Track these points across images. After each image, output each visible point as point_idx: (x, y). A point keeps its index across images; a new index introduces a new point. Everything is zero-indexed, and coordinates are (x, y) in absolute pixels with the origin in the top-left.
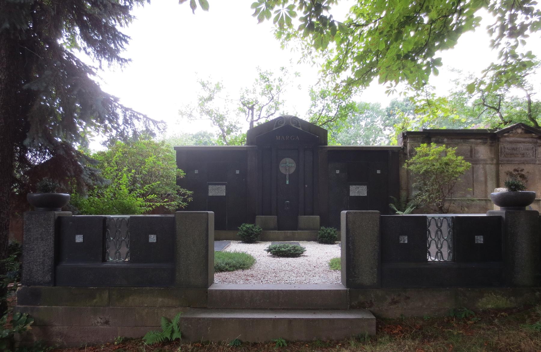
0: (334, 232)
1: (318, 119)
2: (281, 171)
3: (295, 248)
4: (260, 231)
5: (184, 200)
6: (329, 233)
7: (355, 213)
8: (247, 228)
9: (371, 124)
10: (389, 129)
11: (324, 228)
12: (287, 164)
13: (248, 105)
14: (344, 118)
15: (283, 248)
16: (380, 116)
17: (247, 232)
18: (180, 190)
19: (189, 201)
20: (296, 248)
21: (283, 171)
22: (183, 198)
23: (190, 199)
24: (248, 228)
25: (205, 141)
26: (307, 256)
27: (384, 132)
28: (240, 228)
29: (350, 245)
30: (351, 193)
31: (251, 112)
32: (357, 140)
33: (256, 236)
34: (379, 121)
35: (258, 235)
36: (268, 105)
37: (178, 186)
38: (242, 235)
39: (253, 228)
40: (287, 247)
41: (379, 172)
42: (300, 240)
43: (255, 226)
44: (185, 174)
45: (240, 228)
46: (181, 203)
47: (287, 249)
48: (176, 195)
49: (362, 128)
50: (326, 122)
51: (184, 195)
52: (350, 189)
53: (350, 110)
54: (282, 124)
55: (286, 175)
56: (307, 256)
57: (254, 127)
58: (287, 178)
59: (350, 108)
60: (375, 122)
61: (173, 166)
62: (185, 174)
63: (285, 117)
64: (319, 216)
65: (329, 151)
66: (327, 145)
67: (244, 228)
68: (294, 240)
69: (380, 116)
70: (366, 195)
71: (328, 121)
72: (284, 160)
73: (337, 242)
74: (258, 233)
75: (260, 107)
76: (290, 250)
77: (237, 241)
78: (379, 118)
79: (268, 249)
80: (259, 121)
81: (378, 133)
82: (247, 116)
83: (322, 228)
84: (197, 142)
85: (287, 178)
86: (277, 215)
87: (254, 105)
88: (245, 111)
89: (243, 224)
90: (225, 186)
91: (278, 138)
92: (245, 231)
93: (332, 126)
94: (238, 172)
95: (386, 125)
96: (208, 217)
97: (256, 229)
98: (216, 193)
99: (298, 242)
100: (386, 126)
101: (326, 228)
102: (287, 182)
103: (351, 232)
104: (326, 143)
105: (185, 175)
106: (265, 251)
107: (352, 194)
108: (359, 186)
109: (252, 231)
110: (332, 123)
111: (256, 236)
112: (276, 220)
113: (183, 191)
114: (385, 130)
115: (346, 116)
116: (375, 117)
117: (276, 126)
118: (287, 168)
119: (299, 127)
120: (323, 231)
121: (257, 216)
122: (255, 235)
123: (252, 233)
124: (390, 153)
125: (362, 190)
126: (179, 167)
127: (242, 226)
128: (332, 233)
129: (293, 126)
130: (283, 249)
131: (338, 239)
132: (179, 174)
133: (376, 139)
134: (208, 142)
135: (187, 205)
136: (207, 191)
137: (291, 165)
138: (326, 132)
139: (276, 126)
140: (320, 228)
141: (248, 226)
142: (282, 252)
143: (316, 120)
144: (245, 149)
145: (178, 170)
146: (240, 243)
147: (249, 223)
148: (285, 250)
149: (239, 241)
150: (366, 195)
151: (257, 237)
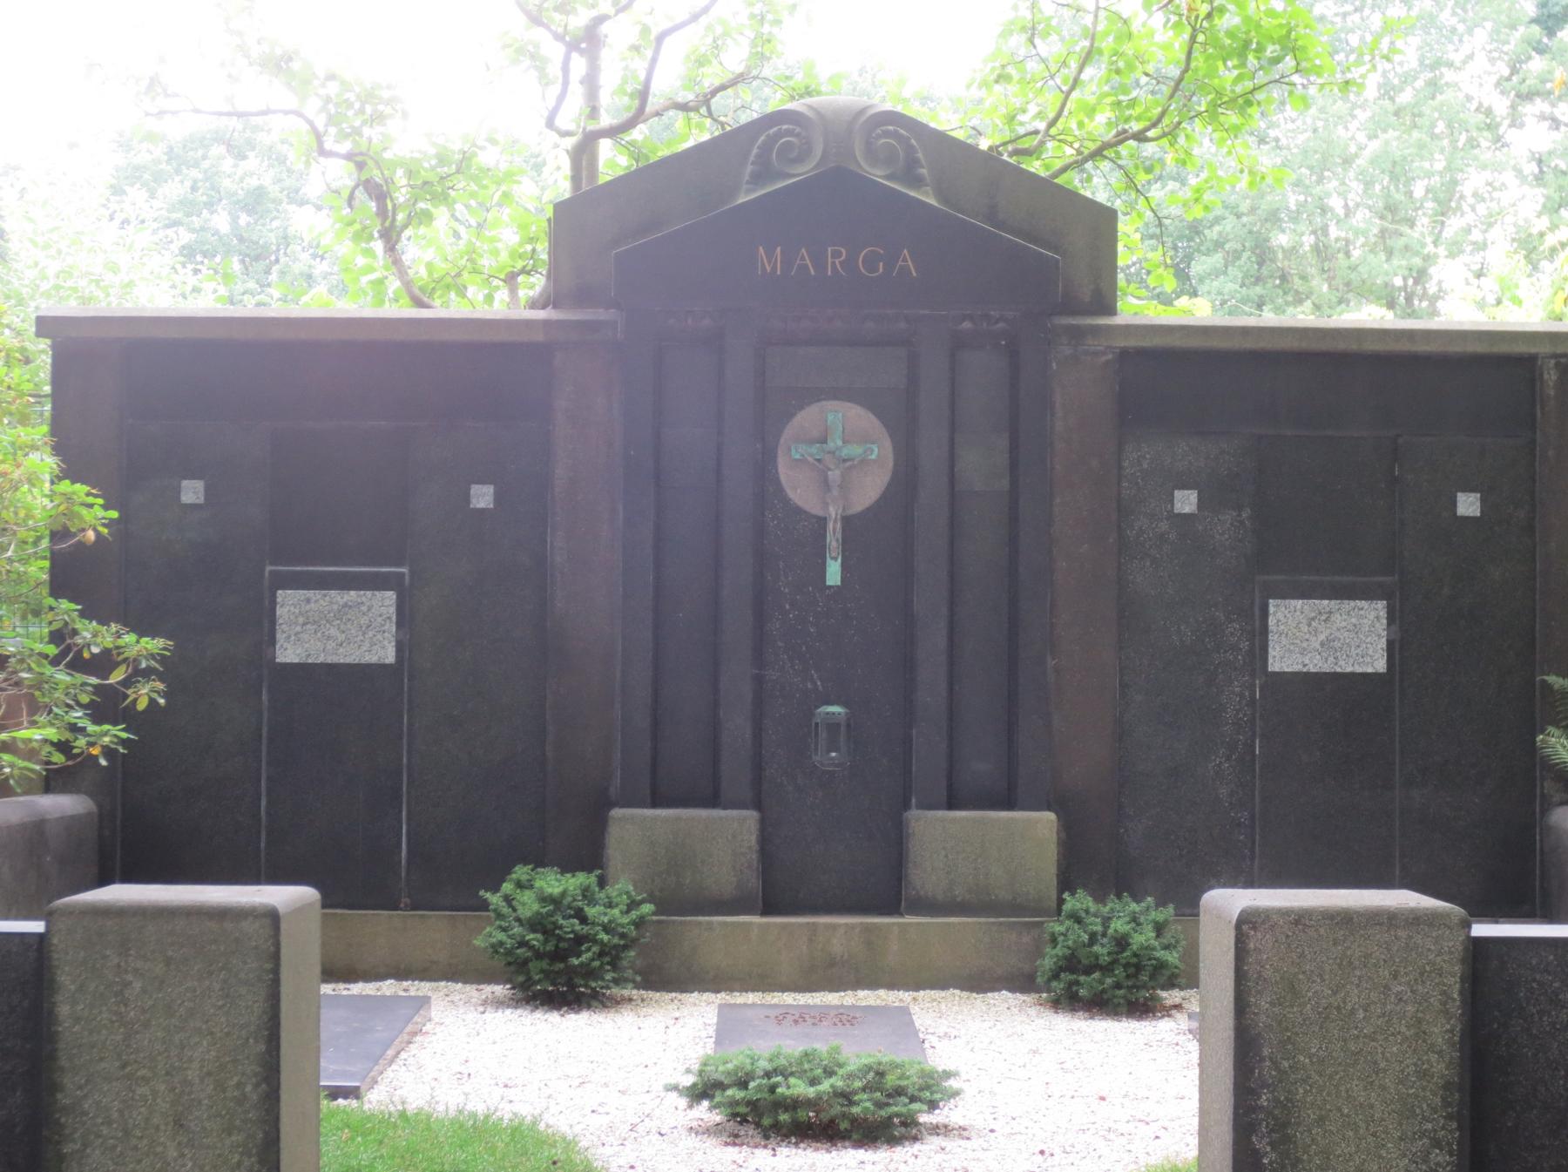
0: (1159, 929)
1: (1052, 123)
2: (791, 494)
3: (881, 1074)
4: (639, 923)
5: (107, 707)
6: (1122, 942)
7: (1297, 922)
8: (544, 899)
9: (1419, 83)
10: (1543, 117)
11: (1089, 903)
12: (831, 445)
13: (557, 16)
14: (1232, 118)
15: (801, 1074)
16: (1489, 25)
17: (545, 932)
18: (75, 632)
19: (142, 705)
20: (891, 1080)
21: (799, 489)
22: (94, 680)
23: (144, 695)
24: (555, 902)
25: (253, 182)
26: (962, 1132)
27: (1511, 135)
28: (495, 899)
29: (1260, 1143)
30: (1274, 652)
31: (579, 65)
32: (1329, 195)
33: (612, 956)
34: (1481, 60)
35: (626, 947)
36: (704, 20)
37: (65, 605)
38: (509, 952)
39: (592, 902)
40: (829, 1073)
41: (1468, 505)
42: (917, 985)
43: (602, 883)
44: (114, 514)
45: (495, 899)
46: (82, 730)
47: (825, 1086)
48: (49, 670)
49: (1363, 107)
50: (1107, 146)
51: (104, 663)
52: (1272, 621)
53: (1276, 61)
54: (800, 160)
55: (822, 522)
56: (962, 1132)
57: (603, 179)
58: (833, 538)
59: (1271, 50)
60: (1450, 65)
61: (34, 457)
62: (114, 514)
63: (818, 113)
64: (1051, 816)
65: (1124, 354)
66: (1111, 310)
67: (528, 905)
68: (873, 985)
69: (1489, 25)
70: (1380, 665)
71: (1122, 137)
72: (807, 418)
73: (1171, 996)
74: (623, 936)
75: (645, 30)
76: (846, 1097)
77: (470, 989)
78: (1481, 36)
79: (689, 1080)
80: (638, 134)
81: (1473, 144)
82: (556, 89)
83: (1071, 903)
84: (194, 189)
85: (833, 538)
86: (758, 805)
87: (601, 19)
88: (537, 59)
89: (521, 872)
90: (390, 597)
91: (768, 261)
92: (535, 924)
93: (1149, 170)
94: (483, 497)
95: (1524, 89)
96: (277, 945)
97: (610, 905)
98: (331, 645)
99: (906, 996)
100: (1528, 96)
101: (1100, 898)
102: (834, 573)
103: (1266, 1052)
104: (1105, 303)
105: (110, 524)
106: (674, 1094)
107: (1283, 658)
108: (1334, 604)
109: (584, 920)
110: (1149, 149)
111: (612, 956)
112: (751, 838)
113: (95, 636)
114: (1516, 122)
115: (1249, 103)
116: (1454, 30)
117: (758, 178)
118: (834, 475)
119: (917, 182)
120: (1079, 921)
121: (616, 813)
122: (601, 955)
123: (579, 940)
124: (1551, 376)
125: (1356, 629)
126: (72, 470)
127: (507, 887)
128: (1143, 938)
129: (877, 174)
130: (798, 1088)
131: (1183, 981)
132: (70, 514)
133: (1454, 182)
134: (274, 191)
135: (123, 742)
136: (264, 625)
137: (855, 450)
138: (1102, 221)
139: (758, 178)
140: (1061, 902)
141: (552, 882)
142: (794, 1104)
143: (1042, 126)
144: (539, 337)
145: (65, 486)
146: (499, 1004)
147: (568, 867)
148: (811, 1092)
149: (489, 989)
150: (1380, 665)
151: (614, 966)
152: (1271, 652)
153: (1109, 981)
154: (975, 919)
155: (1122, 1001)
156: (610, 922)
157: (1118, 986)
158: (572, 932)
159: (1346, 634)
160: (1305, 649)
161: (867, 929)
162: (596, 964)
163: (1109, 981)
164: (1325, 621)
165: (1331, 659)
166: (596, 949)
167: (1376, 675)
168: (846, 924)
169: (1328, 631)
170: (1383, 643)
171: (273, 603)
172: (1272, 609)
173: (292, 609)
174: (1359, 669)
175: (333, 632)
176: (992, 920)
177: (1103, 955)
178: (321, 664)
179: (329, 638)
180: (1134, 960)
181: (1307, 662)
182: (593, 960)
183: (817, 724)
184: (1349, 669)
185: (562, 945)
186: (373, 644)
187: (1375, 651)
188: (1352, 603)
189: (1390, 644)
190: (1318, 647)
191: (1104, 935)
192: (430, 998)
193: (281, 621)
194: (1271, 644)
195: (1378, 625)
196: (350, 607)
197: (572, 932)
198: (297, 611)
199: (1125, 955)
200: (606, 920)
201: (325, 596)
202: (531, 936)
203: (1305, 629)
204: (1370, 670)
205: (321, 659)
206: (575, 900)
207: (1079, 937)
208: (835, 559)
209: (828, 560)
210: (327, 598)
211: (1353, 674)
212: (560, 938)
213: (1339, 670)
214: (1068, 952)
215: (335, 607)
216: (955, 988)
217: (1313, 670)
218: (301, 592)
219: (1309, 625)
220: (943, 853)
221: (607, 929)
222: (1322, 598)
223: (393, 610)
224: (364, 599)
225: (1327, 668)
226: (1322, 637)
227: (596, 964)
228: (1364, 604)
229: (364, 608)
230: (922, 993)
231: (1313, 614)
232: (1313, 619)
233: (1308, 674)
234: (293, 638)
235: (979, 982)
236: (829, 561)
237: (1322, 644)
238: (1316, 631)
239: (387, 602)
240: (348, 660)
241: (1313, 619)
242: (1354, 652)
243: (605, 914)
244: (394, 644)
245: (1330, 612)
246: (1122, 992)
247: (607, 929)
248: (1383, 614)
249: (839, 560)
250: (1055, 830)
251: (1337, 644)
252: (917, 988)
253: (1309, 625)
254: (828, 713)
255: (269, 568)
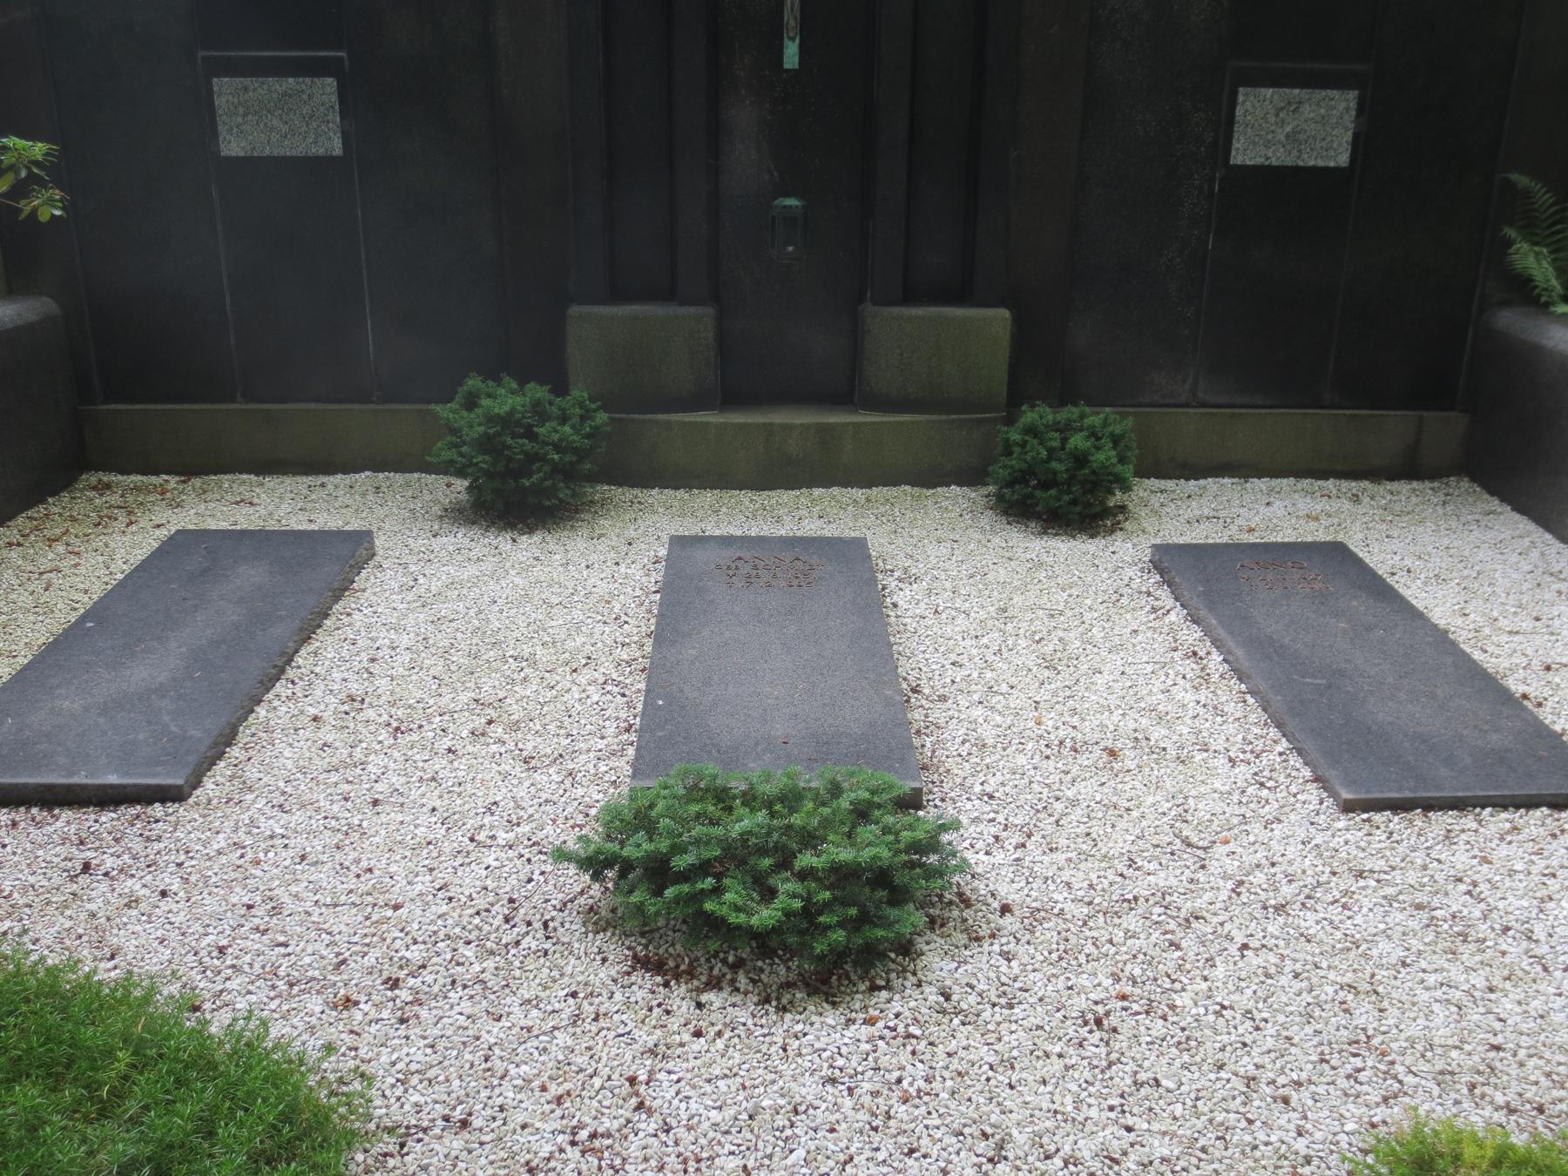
6: (1081, 459)
8: (491, 419)
24: (507, 422)
30: (1238, 144)
39: (544, 417)
52: (1239, 111)
64: (1004, 313)
70: (1343, 159)
98: (275, 137)
121: (574, 310)
123: (532, 458)
141: (507, 399)
152: (1236, 145)
153: (1066, 498)
154: (927, 417)
155: (1076, 517)
156: (561, 440)
157: (1074, 502)
158: (522, 452)
159: (1312, 126)
160: (1269, 141)
161: (823, 429)
162: (548, 483)
163: (1066, 498)
164: (1294, 111)
165: (1295, 152)
166: (547, 469)
167: (1336, 170)
168: (802, 425)
169: (1295, 123)
170: (1349, 136)
171: (210, 92)
172: (1241, 98)
173: (230, 97)
174: (1321, 163)
175: (275, 122)
176: (944, 417)
177: (1061, 472)
178: (268, 157)
179: (272, 130)
180: (1093, 478)
181: (1270, 154)
182: (545, 479)
183: (773, 217)
184: (1312, 163)
185: (512, 465)
186: (318, 136)
187: (1340, 145)
188: (1324, 93)
189: (1356, 136)
190: (1283, 139)
191: (1063, 448)
192: (369, 534)
193: (220, 112)
194: (1236, 135)
195: (1346, 117)
196: (290, 96)
197: (522, 452)
198: (236, 101)
199: (1083, 472)
200: (556, 437)
201: (263, 83)
202: (480, 458)
203: (1272, 119)
204: (1332, 164)
205: (267, 152)
206: (524, 417)
207: (1039, 453)
208: (793, 39)
209: (786, 40)
210: (265, 87)
211: (1315, 169)
212: (510, 459)
213: (1301, 164)
214: (1024, 466)
215: (275, 96)
216: (906, 484)
217: (1274, 163)
218: (238, 80)
219: (1277, 115)
220: (898, 351)
221: (557, 447)
222: (1293, 86)
223: (334, 98)
224: (304, 86)
225: (1289, 161)
226: (1288, 129)
227: (548, 483)
228: (1335, 93)
229: (305, 97)
230: (875, 491)
231: (1282, 104)
232: (1282, 109)
233: (1270, 167)
234: (235, 130)
235: (929, 477)
236: (787, 42)
237: (1287, 136)
238: (1283, 121)
239: (328, 90)
240: (294, 153)
241: (1282, 109)
242: (1318, 145)
243: (556, 431)
244: (339, 135)
245: (1300, 102)
246: (1078, 509)
247: (557, 447)
248: (1353, 105)
249: (797, 41)
250: (1009, 328)
251: (1302, 137)
252: (869, 485)
253: (1277, 115)
254: (785, 207)
255: (201, 54)
